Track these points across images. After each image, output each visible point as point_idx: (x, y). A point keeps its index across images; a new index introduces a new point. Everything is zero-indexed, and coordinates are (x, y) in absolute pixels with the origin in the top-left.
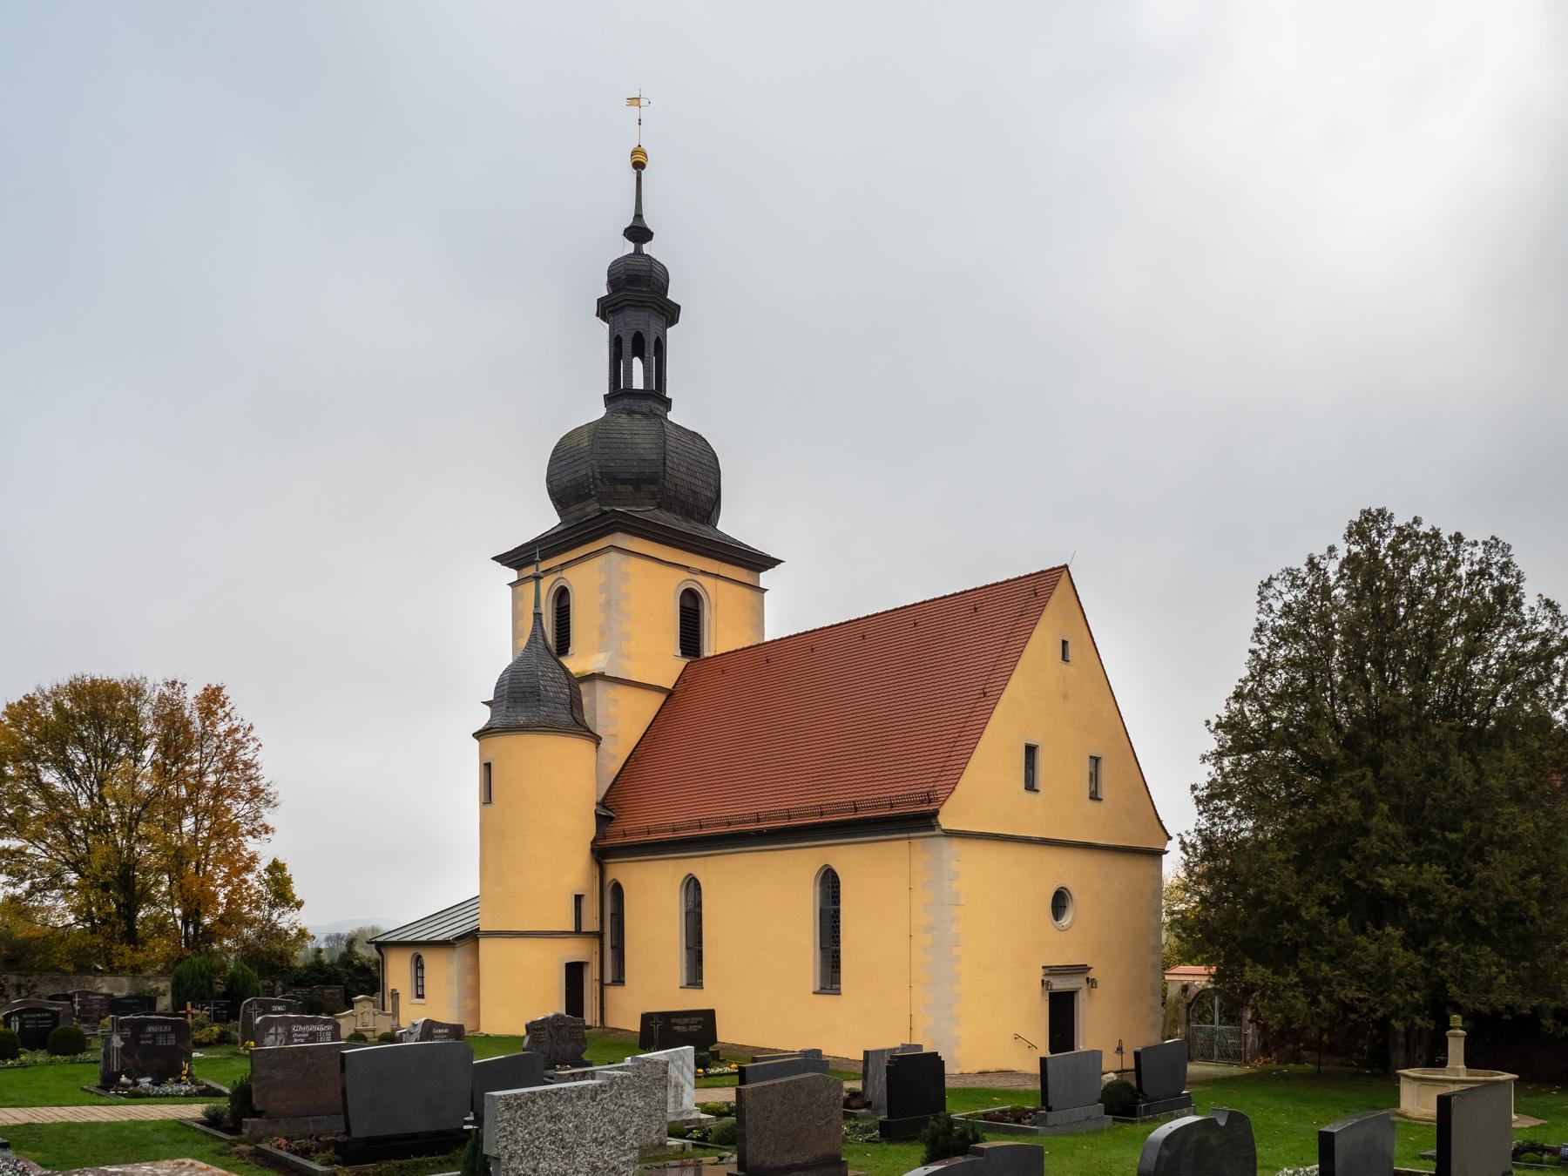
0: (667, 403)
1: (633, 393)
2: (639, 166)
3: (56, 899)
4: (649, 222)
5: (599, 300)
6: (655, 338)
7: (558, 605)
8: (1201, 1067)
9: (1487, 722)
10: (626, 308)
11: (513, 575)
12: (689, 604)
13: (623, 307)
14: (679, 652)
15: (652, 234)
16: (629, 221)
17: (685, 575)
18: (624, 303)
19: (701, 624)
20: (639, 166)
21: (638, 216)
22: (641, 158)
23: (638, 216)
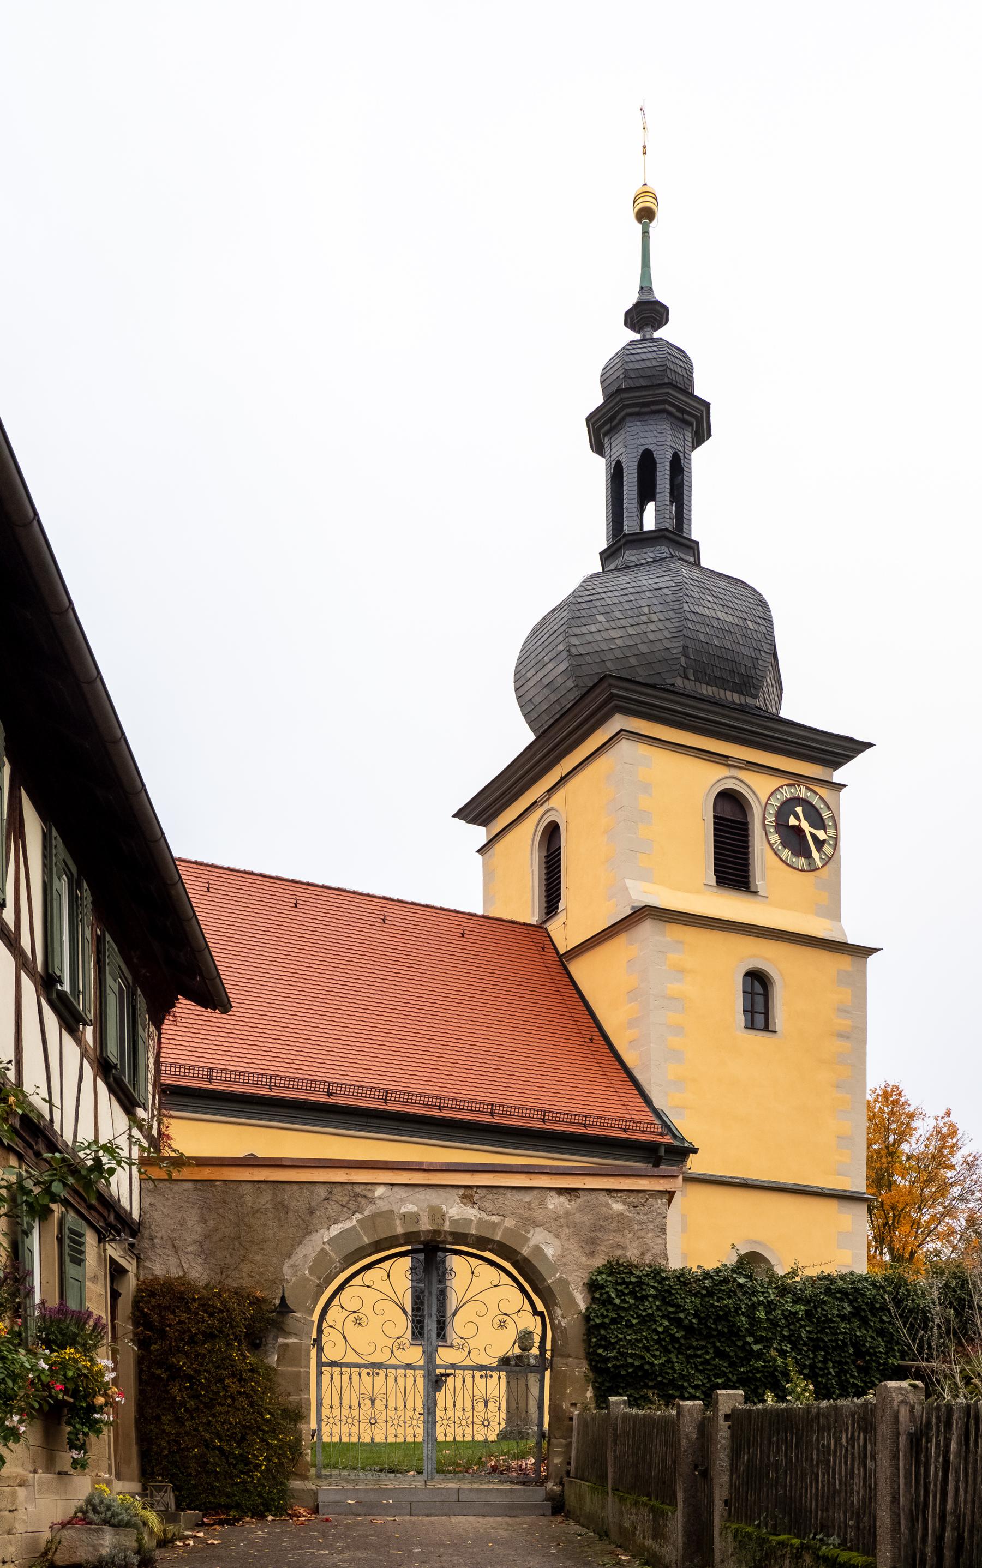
0: (693, 548)
1: (647, 539)
2: (646, 215)
3: (593, 1320)
4: (660, 294)
5: (588, 420)
6: (669, 455)
7: (548, 850)
8: (120, 1441)
9: (784, 1336)
10: (628, 419)
11: (480, 834)
12: (729, 812)
13: (623, 419)
14: (713, 880)
15: (666, 309)
16: (631, 298)
17: (721, 772)
18: (623, 414)
19: (751, 867)
20: (646, 215)
21: (646, 288)
22: (647, 202)
23: (646, 288)
